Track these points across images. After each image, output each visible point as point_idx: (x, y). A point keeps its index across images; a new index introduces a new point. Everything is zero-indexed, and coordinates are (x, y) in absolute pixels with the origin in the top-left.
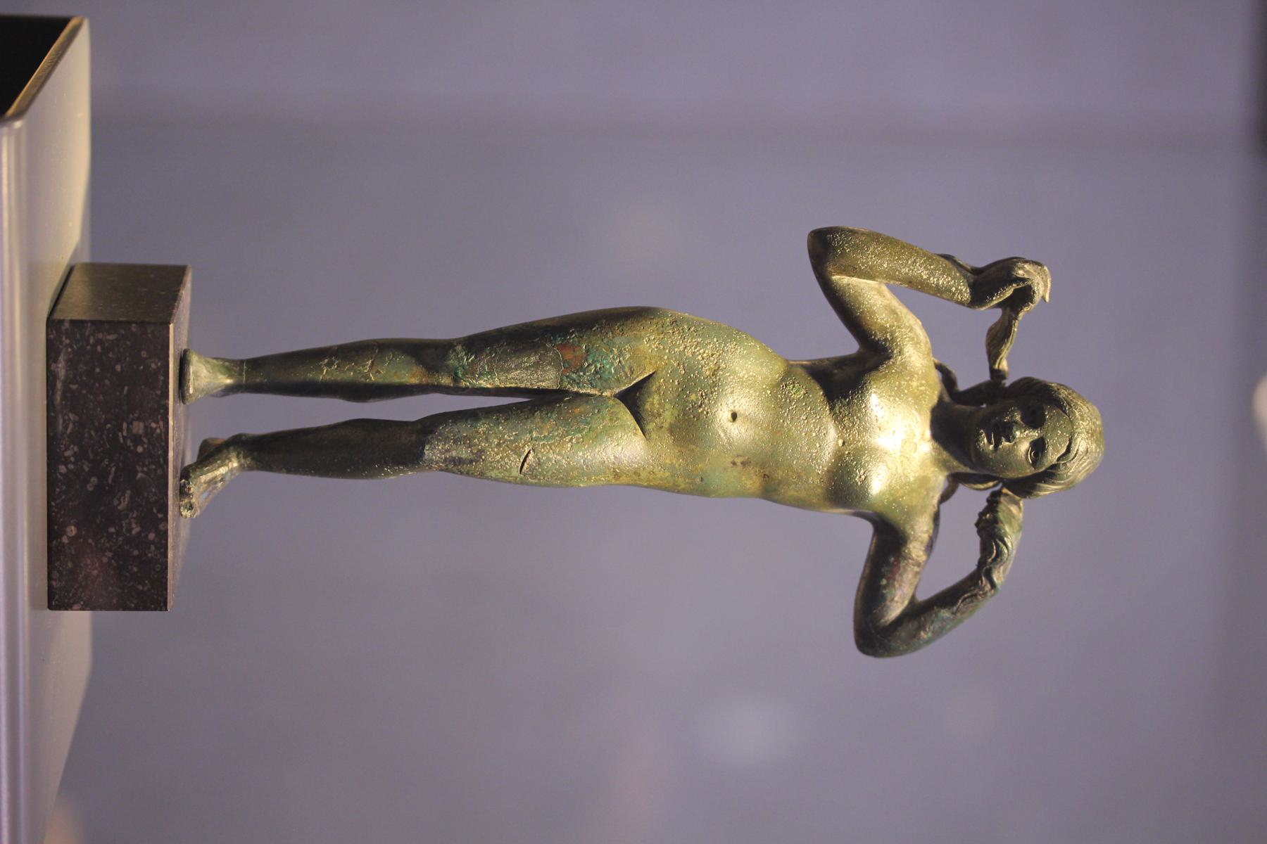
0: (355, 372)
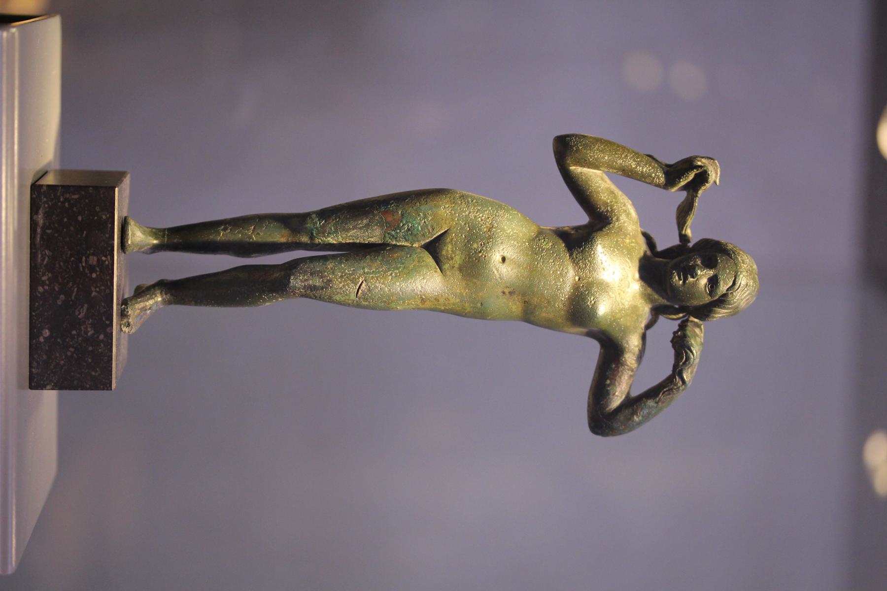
0: (242, 234)
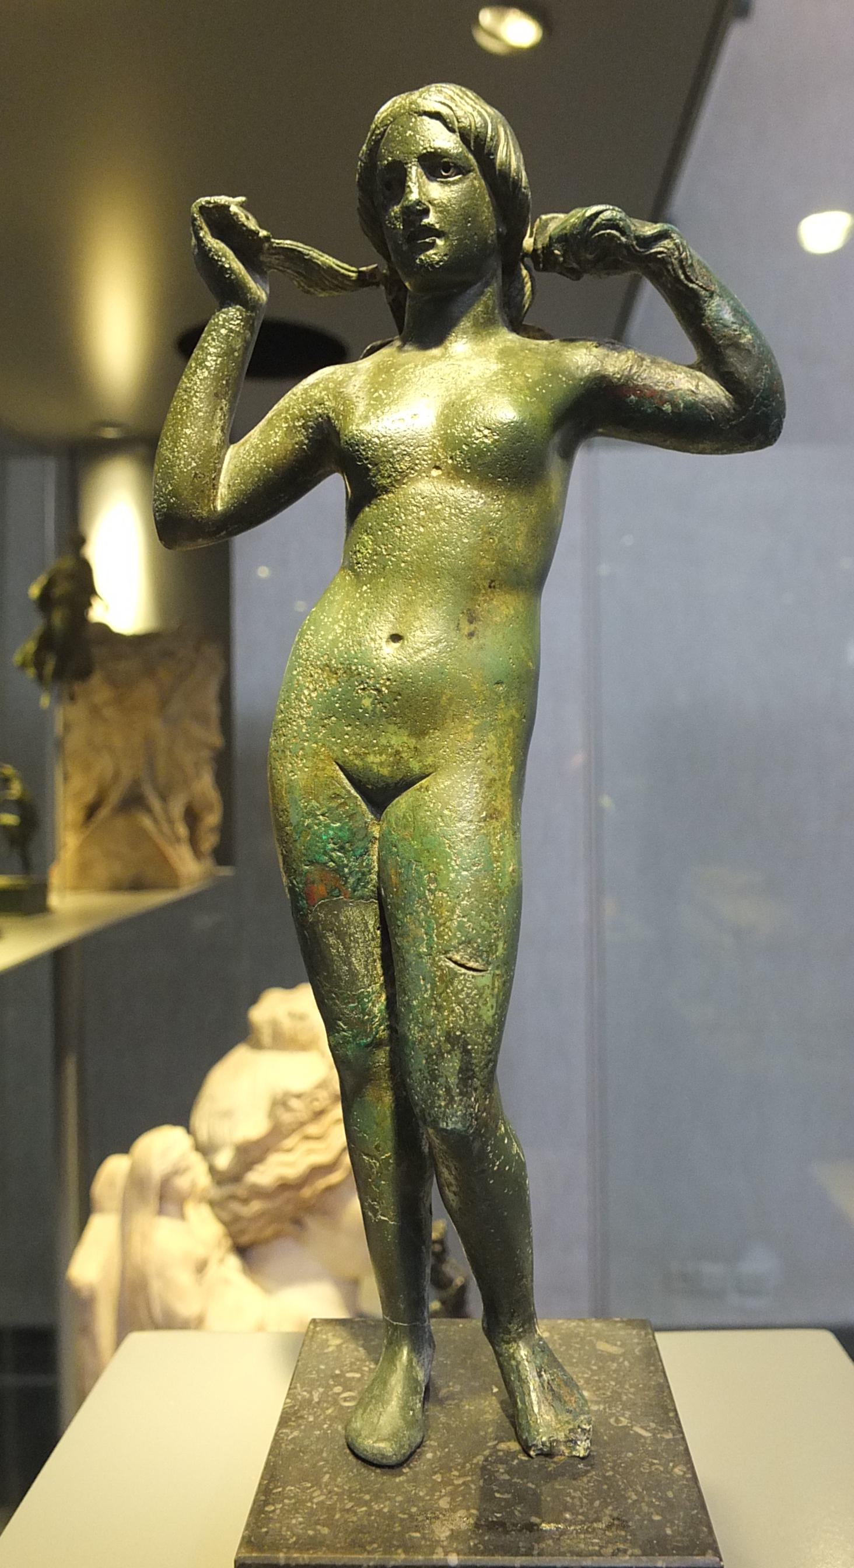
0: (380, 1179)
